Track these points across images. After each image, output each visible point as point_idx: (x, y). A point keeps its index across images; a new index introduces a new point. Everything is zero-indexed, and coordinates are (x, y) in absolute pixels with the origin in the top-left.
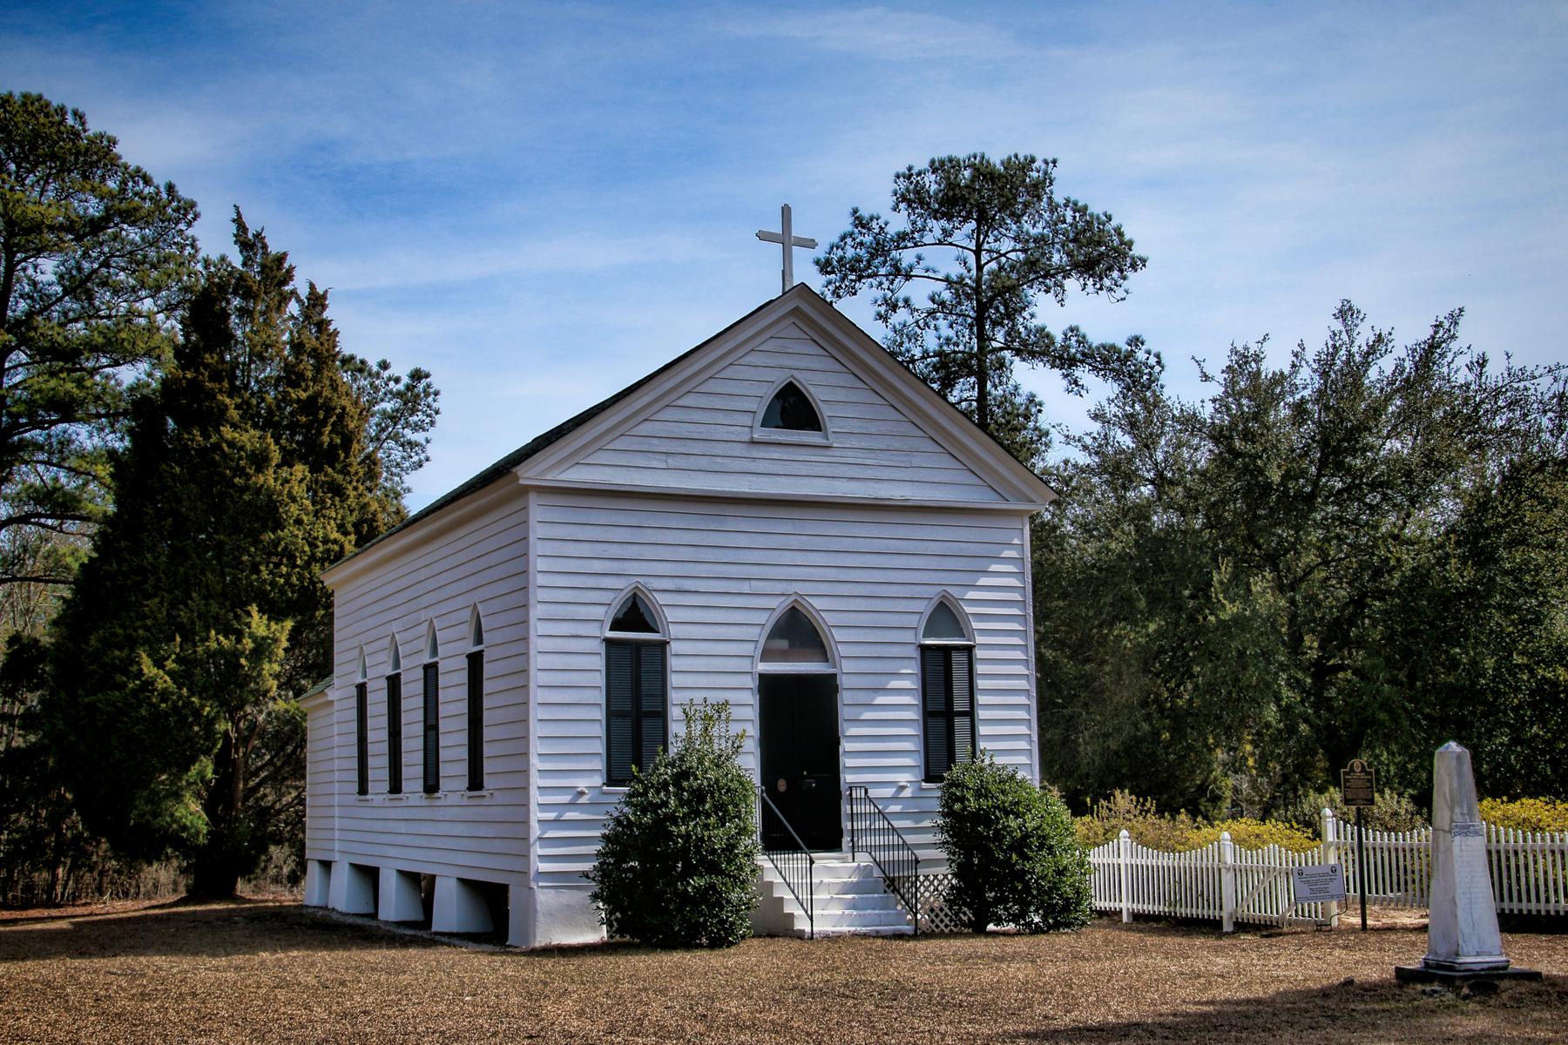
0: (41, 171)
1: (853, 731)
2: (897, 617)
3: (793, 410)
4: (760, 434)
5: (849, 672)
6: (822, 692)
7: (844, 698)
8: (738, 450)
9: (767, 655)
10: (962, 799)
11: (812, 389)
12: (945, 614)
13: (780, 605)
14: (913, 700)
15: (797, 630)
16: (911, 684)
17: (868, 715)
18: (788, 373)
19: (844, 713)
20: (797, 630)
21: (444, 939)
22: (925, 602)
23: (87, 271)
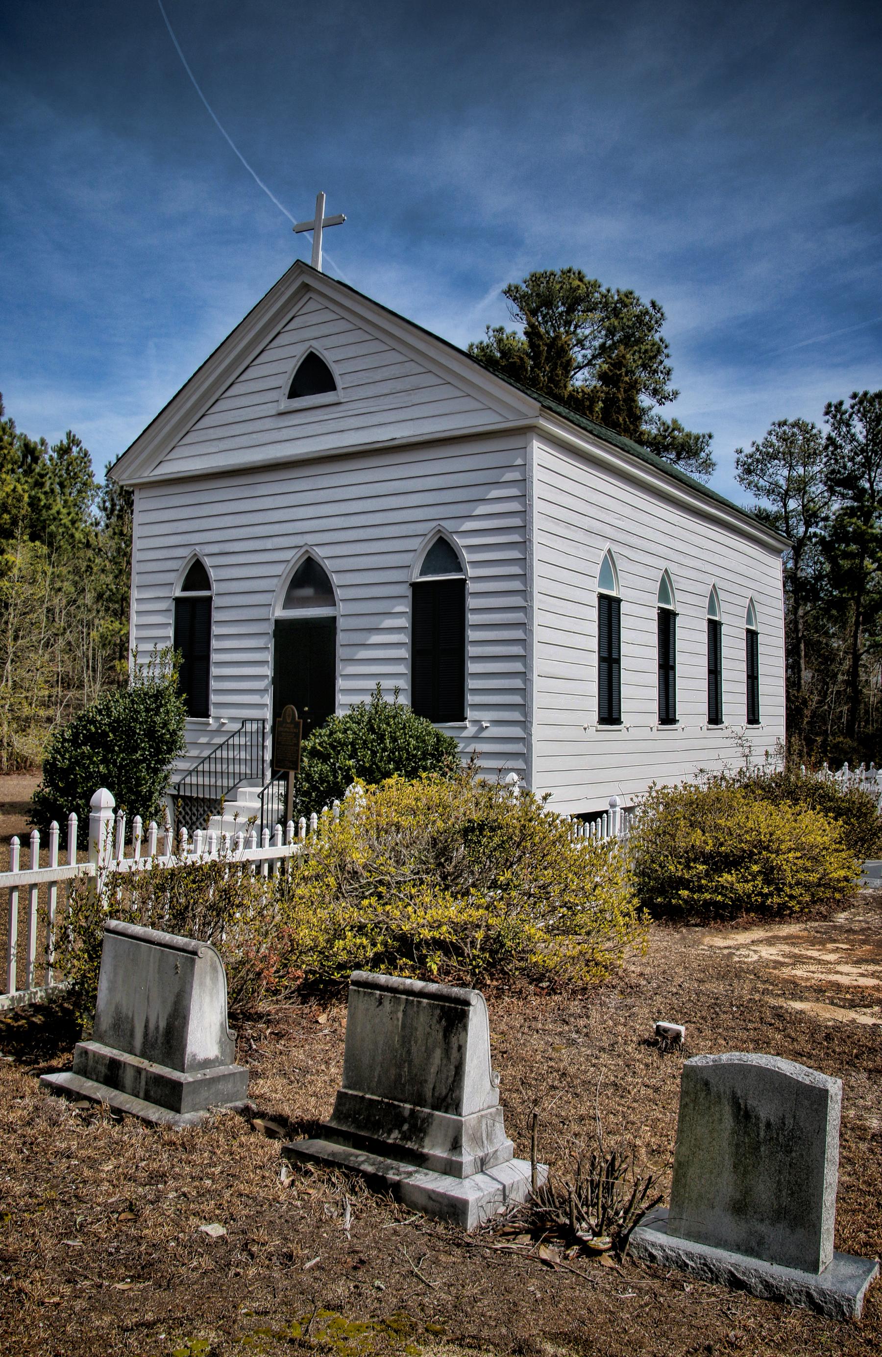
0: (645, 400)
1: (351, 669)
2: (277, 526)
3: (313, 377)
4: (285, 404)
5: (344, 610)
6: (325, 629)
7: (341, 638)
8: (269, 423)
9: (289, 603)
10: (673, 837)
11: (325, 353)
12: (443, 552)
13: (293, 558)
14: (405, 638)
15: (310, 578)
16: (405, 622)
17: (363, 654)
18: (307, 344)
19: (341, 653)
20: (310, 578)
21: (454, 1053)
22: (420, 539)
23: (777, 524)
